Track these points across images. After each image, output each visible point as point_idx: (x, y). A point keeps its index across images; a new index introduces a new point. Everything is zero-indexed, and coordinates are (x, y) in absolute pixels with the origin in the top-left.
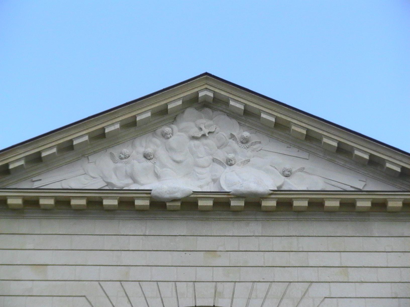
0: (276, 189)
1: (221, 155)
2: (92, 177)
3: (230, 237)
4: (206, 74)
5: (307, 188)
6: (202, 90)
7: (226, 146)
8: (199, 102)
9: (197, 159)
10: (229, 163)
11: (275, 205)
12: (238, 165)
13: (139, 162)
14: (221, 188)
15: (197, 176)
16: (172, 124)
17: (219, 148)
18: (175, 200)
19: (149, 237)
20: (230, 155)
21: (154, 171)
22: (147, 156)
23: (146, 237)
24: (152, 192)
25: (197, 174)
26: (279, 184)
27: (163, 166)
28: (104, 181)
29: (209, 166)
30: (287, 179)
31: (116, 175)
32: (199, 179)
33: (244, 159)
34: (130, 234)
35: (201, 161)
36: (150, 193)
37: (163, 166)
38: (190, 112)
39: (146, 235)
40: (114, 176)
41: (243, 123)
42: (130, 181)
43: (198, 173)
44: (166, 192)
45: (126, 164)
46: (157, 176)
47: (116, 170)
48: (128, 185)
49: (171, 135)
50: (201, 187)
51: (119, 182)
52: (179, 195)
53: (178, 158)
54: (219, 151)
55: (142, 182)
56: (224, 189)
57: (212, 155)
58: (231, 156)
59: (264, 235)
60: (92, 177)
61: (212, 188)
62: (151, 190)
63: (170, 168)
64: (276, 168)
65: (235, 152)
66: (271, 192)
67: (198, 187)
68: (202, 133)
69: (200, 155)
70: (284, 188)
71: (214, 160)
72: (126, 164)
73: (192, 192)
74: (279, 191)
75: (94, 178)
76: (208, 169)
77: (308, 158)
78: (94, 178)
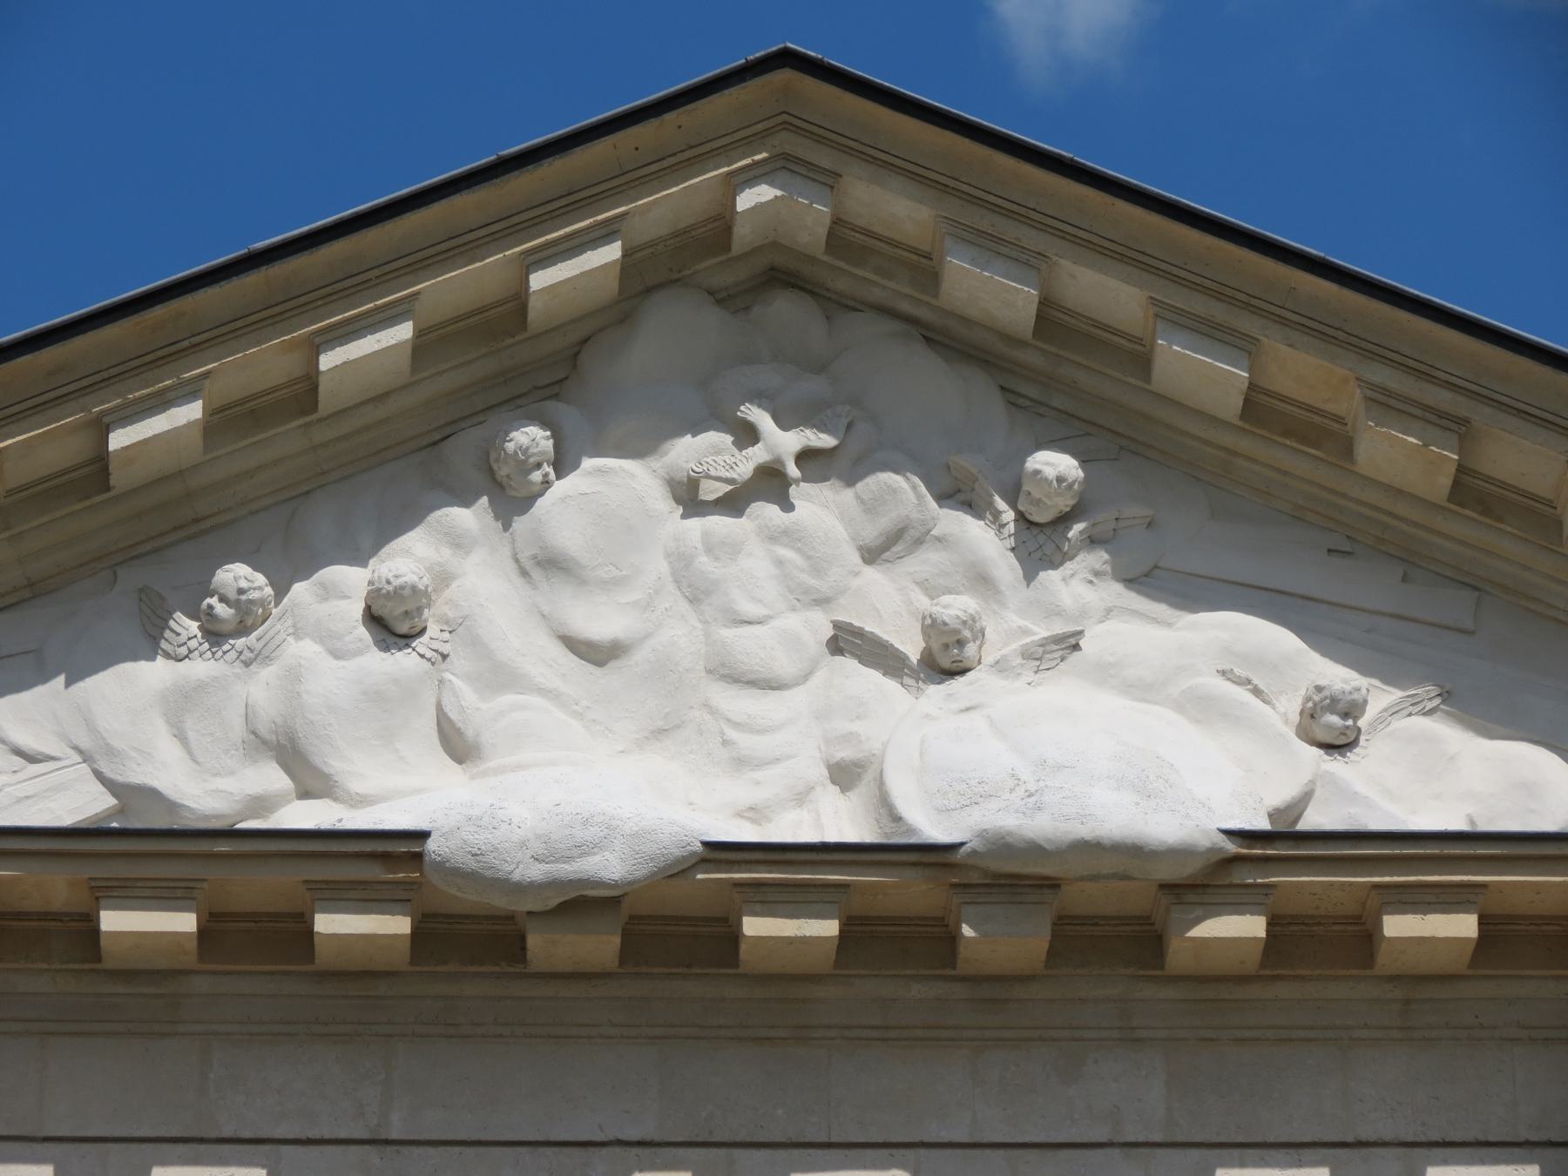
0: (1263, 824)
1: (892, 606)
2: (19, 752)
3: (959, 1152)
4: (600, 664)
5: (1472, 823)
6: (751, 177)
7: (919, 542)
8: (737, 247)
9: (729, 634)
10: (944, 661)
11: (1263, 934)
12: (1000, 667)
13: (337, 654)
14: (897, 819)
15: (725, 743)
16: (556, 397)
17: (872, 555)
18: (582, 903)
19: (405, 1150)
20: (946, 599)
21: (440, 708)
22: (390, 624)
23: (390, 1149)
24: (432, 845)
25: (731, 734)
26: (1280, 794)
27: (500, 677)
28: (99, 776)
29: (805, 677)
30: (1334, 765)
31: (182, 738)
32: (742, 763)
33: (1042, 632)
34: (279, 1133)
35: (755, 646)
36: (419, 856)
37: (500, 677)
38: (677, 329)
39: (387, 1142)
40: (167, 747)
41: (1032, 391)
42: (271, 778)
43: (737, 725)
44: (523, 844)
45: (247, 664)
46: (458, 745)
47: (180, 707)
48: (262, 804)
49: (550, 470)
50: (753, 813)
51: (209, 784)
52: (610, 866)
53: (599, 620)
54: (872, 575)
55: (356, 786)
56: (911, 830)
57: (822, 602)
58: (956, 606)
59: (1181, 1138)
60: (19, 752)
61: (841, 821)
62: (423, 835)
63: (542, 691)
64: (1257, 692)
65: (981, 581)
66: (1231, 847)
67: (740, 815)
68: (757, 455)
69: (749, 608)
70: (1315, 819)
71: (847, 641)
72: (247, 664)
73: (698, 847)
74: (1279, 843)
75: (31, 758)
76: (797, 698)
77: (1468, 624)
78: (31, 758)
